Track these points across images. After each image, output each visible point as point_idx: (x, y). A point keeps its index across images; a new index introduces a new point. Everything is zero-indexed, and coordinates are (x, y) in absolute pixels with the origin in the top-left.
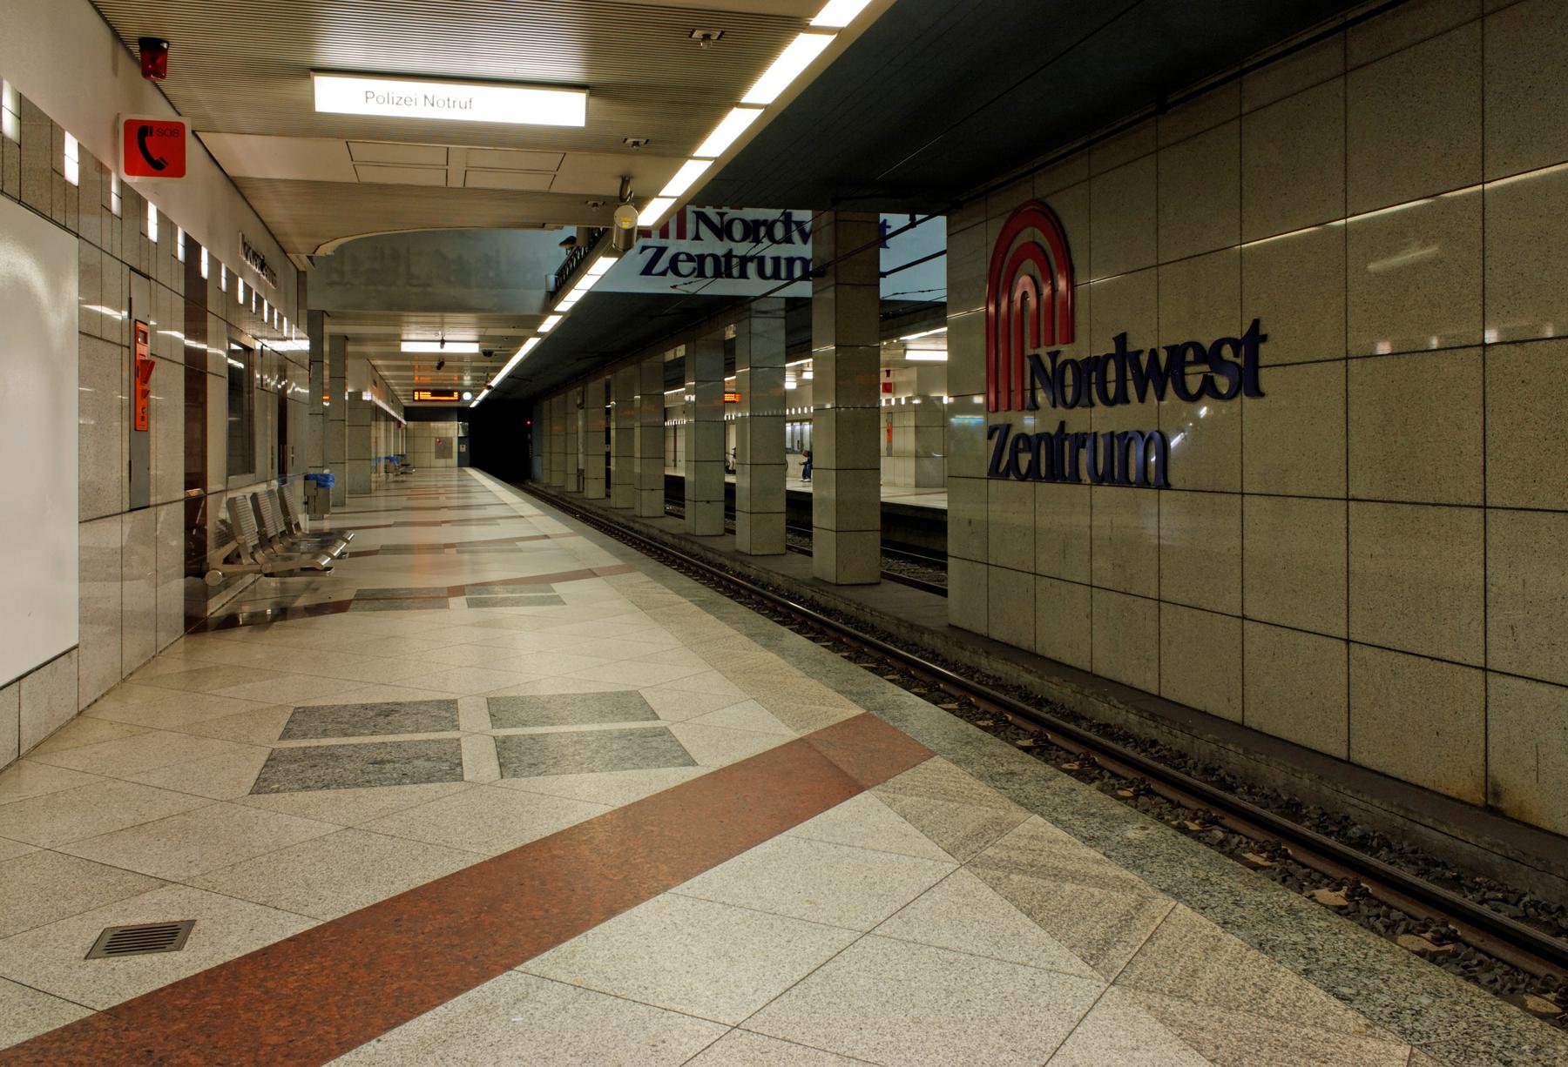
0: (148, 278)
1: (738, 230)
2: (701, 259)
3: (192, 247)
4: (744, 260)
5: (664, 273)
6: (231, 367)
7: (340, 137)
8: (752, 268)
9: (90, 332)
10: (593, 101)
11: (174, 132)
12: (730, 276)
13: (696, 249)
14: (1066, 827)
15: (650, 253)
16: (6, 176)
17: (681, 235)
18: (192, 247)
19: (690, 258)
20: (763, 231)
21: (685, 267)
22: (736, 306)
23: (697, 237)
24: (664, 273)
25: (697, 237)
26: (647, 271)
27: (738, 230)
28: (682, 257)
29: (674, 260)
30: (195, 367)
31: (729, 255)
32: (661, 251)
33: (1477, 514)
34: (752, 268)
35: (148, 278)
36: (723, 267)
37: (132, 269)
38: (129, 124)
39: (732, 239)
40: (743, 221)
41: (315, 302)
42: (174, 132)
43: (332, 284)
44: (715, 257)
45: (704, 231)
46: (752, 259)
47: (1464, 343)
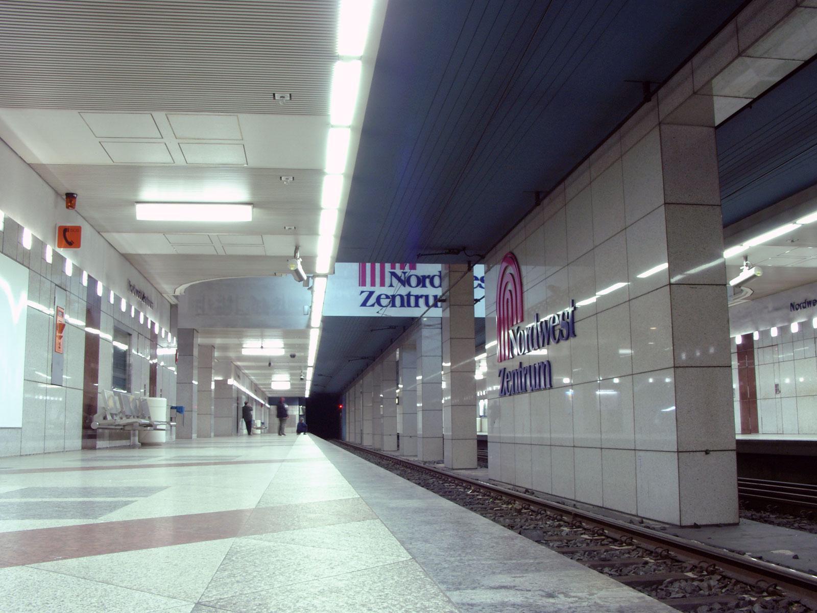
0: (66, 290)
1: (414, 281)
2: (394, 297)
3: (92, 282)
4: (417, 298)
5: (373, 305)
6: (115, 348)
7: (161, 233)
8: (422, 301)
9: (32, 317)
10: (255, 209)
11: (77, 230)
12: (409, 305)
13: (390, 292)
14: (58, 559)
15: (365, 295)
16: (2, 243)
17: (382, 284)
18: (92, 282)
19: (387, 297)
20: (427, 281)
21: (384, 302)
22: (411, 324)
23: (391, 286)
24: (373, 305)
25: (391, 286)
26: (364, 304)
27: (414, 281)
28: (383, 296)
29: (379, 298)
30: (92, 346)
31: (409, 295)
32: (371, 293)
33: (798, 396)
34: (422, 301)
35: (66, 290)
36: (406, 301)
37: (56, 285)
38: (60, 228)
39: (410, 285)
40: (416, 276)
41: (185, 324)
42: (77, 230)
43: (198, 315)
44: (401, 296)
45: (395, 282)
46: (421, 296)
47: (609, 241)
